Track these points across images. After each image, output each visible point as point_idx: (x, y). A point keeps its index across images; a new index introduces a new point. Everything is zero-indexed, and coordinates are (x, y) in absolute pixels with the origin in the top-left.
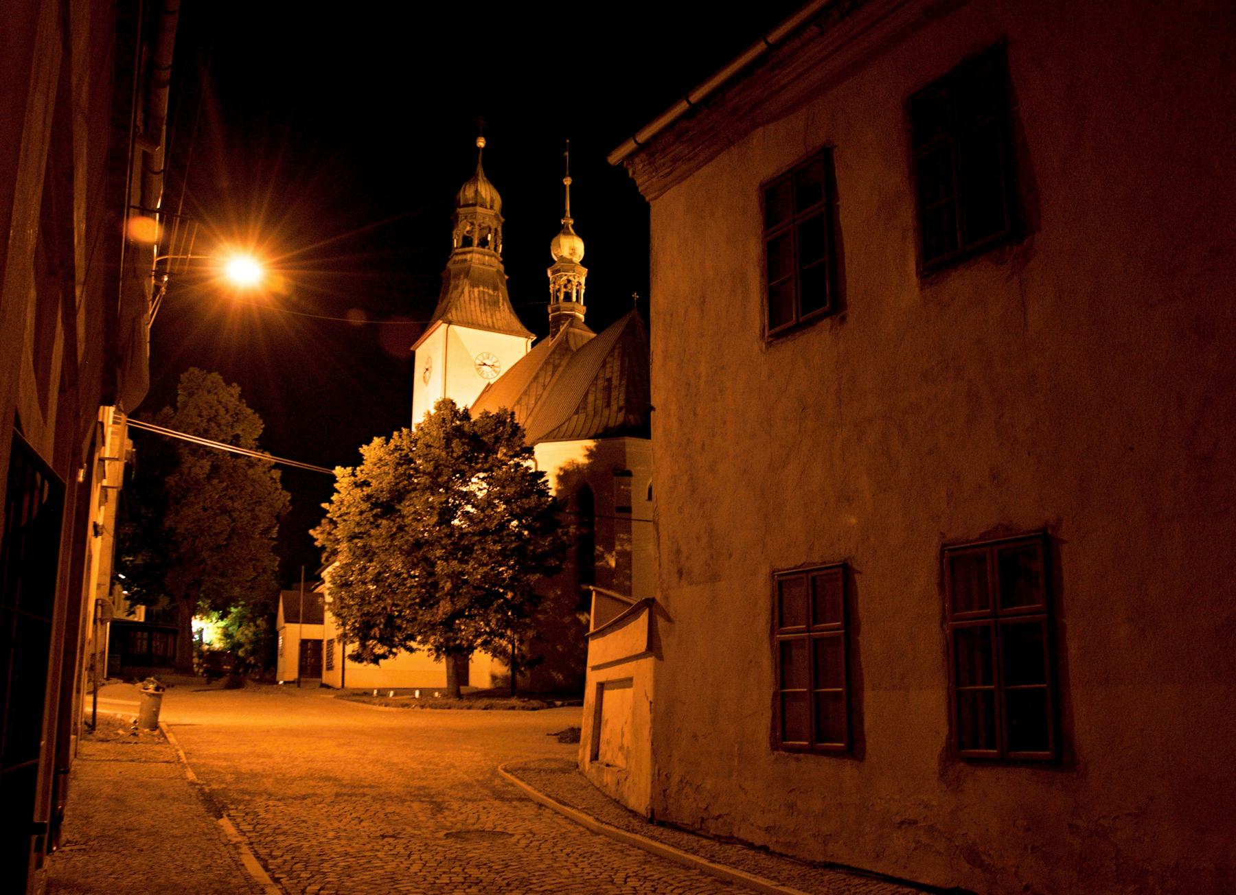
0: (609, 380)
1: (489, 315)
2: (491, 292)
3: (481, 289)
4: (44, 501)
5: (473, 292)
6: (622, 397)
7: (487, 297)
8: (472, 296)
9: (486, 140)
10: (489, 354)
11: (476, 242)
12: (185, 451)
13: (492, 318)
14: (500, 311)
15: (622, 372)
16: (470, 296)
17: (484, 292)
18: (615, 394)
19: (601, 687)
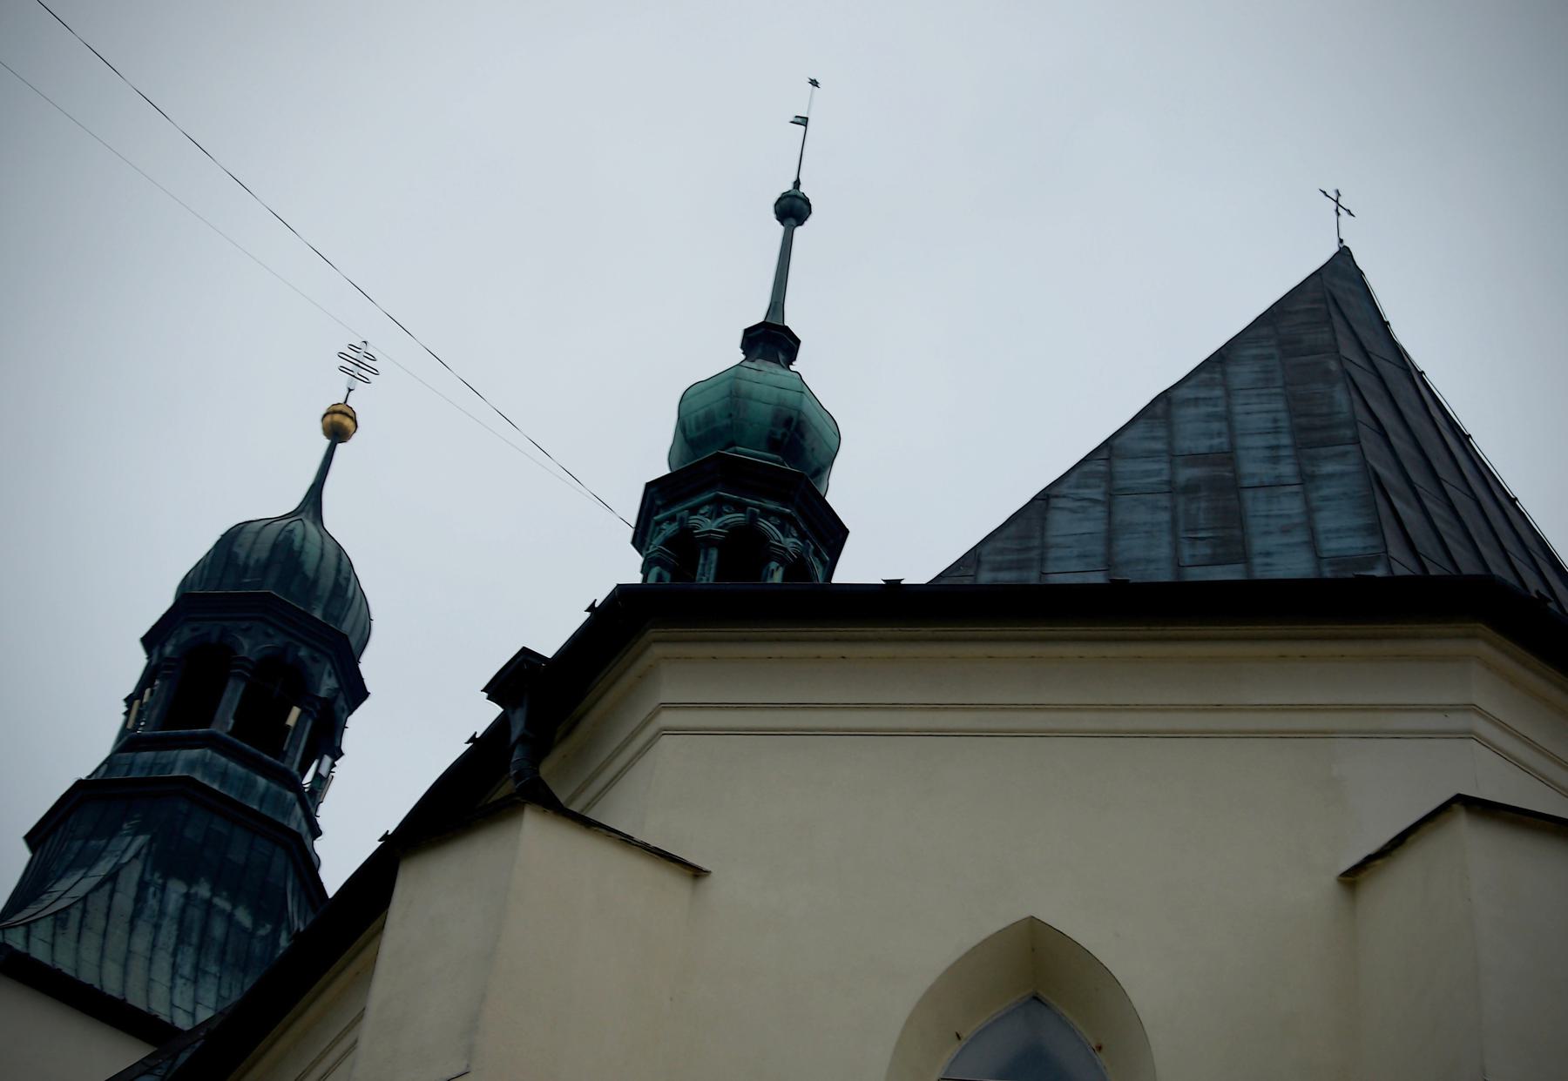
2: (243, 917)
3: (204, 891)
4: (277, 956)
5: (163, 888)
7: (218, 929)
8: (152, 902)
9: (328, 755)
16: (140, 899)
17: (209, 904)
19: (301, 520)
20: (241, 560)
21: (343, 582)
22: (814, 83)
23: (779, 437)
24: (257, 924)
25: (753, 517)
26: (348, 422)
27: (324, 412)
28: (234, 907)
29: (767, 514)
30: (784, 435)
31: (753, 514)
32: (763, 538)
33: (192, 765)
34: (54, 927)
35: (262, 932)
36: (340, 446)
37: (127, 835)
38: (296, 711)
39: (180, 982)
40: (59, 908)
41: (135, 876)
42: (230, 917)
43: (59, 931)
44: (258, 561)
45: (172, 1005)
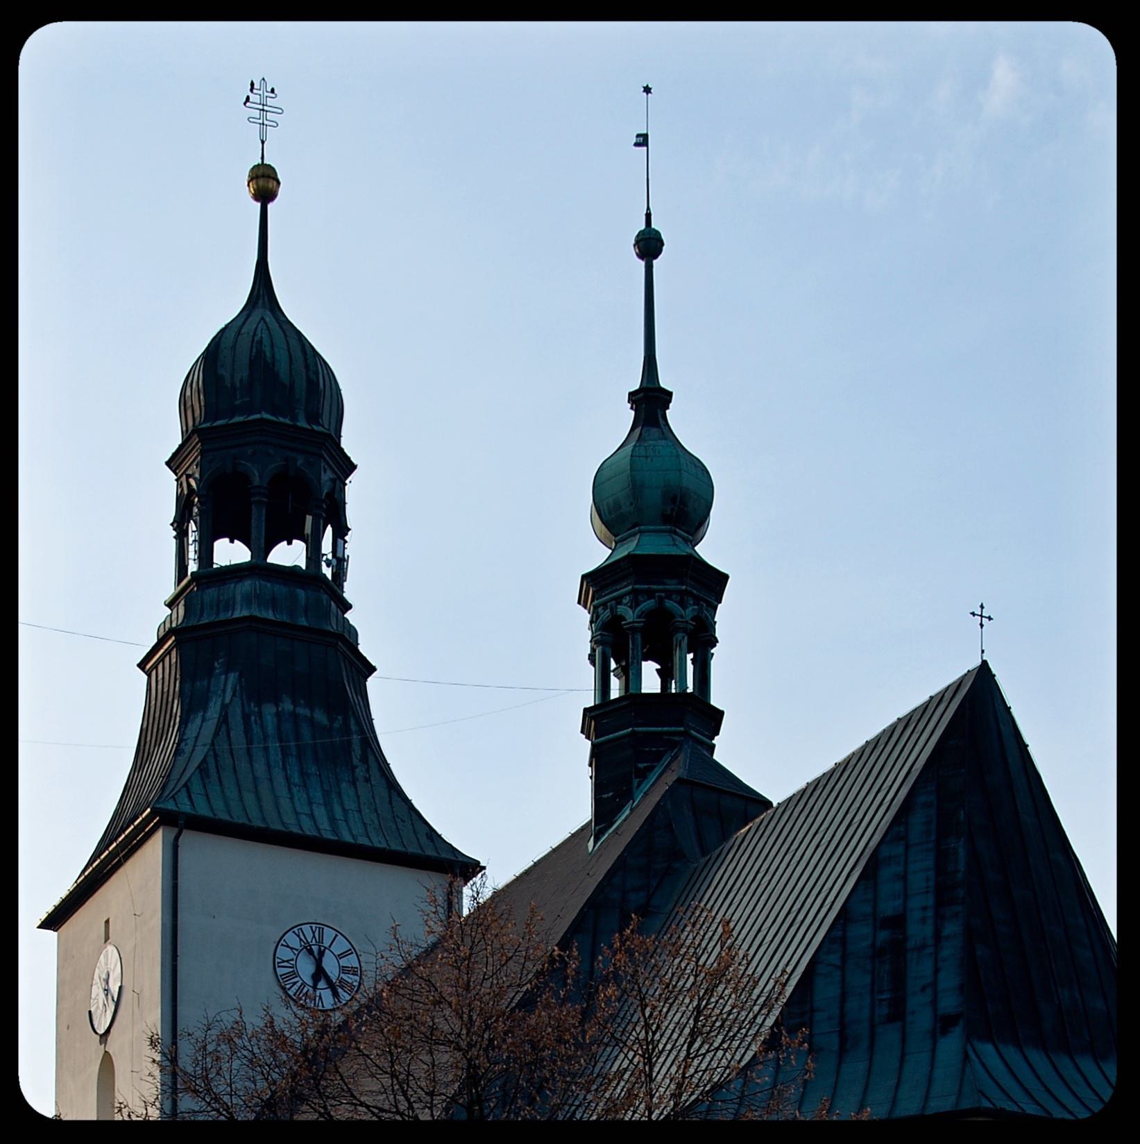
0: (897, 922)
1: (318, 795)
2: (320, 717)
3: (287, 706)
5: (260, 714)
6: (949, 980)
7: (306, 732)
8: (256, 729)
10: (321, 927)
11: (298, 743)
12: (598, 782)
13: (328, 805)
14: (354, 783)
15: (943, 895)
16: (247, 731)
17: (294, 716)
18: (919, 970)
20: (228, 383)
21: (313, 376)
22: (647, 90)
23: (669, 512)
24: (332, 720)
25: (661, 600)
26: (272, 184)
27: (246, 183)
28: (312, 710)
29: (669, 593)
30: (672, 510)
31: (660, 598)
32: (670, 615)
33: (248, 600)
34: (202, 779)
35: (336, 725)
36: (271, 207)
37: (221, 674)
38: (309, 519)
39: (295, 790)
40: (199, 762)
41: (239, 711)
42: (311, 722)
43: (207, 781)
44: (241, 380)
45: (297, 813)
